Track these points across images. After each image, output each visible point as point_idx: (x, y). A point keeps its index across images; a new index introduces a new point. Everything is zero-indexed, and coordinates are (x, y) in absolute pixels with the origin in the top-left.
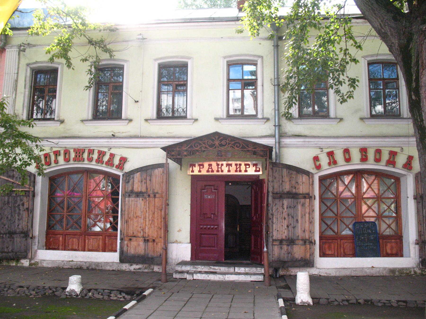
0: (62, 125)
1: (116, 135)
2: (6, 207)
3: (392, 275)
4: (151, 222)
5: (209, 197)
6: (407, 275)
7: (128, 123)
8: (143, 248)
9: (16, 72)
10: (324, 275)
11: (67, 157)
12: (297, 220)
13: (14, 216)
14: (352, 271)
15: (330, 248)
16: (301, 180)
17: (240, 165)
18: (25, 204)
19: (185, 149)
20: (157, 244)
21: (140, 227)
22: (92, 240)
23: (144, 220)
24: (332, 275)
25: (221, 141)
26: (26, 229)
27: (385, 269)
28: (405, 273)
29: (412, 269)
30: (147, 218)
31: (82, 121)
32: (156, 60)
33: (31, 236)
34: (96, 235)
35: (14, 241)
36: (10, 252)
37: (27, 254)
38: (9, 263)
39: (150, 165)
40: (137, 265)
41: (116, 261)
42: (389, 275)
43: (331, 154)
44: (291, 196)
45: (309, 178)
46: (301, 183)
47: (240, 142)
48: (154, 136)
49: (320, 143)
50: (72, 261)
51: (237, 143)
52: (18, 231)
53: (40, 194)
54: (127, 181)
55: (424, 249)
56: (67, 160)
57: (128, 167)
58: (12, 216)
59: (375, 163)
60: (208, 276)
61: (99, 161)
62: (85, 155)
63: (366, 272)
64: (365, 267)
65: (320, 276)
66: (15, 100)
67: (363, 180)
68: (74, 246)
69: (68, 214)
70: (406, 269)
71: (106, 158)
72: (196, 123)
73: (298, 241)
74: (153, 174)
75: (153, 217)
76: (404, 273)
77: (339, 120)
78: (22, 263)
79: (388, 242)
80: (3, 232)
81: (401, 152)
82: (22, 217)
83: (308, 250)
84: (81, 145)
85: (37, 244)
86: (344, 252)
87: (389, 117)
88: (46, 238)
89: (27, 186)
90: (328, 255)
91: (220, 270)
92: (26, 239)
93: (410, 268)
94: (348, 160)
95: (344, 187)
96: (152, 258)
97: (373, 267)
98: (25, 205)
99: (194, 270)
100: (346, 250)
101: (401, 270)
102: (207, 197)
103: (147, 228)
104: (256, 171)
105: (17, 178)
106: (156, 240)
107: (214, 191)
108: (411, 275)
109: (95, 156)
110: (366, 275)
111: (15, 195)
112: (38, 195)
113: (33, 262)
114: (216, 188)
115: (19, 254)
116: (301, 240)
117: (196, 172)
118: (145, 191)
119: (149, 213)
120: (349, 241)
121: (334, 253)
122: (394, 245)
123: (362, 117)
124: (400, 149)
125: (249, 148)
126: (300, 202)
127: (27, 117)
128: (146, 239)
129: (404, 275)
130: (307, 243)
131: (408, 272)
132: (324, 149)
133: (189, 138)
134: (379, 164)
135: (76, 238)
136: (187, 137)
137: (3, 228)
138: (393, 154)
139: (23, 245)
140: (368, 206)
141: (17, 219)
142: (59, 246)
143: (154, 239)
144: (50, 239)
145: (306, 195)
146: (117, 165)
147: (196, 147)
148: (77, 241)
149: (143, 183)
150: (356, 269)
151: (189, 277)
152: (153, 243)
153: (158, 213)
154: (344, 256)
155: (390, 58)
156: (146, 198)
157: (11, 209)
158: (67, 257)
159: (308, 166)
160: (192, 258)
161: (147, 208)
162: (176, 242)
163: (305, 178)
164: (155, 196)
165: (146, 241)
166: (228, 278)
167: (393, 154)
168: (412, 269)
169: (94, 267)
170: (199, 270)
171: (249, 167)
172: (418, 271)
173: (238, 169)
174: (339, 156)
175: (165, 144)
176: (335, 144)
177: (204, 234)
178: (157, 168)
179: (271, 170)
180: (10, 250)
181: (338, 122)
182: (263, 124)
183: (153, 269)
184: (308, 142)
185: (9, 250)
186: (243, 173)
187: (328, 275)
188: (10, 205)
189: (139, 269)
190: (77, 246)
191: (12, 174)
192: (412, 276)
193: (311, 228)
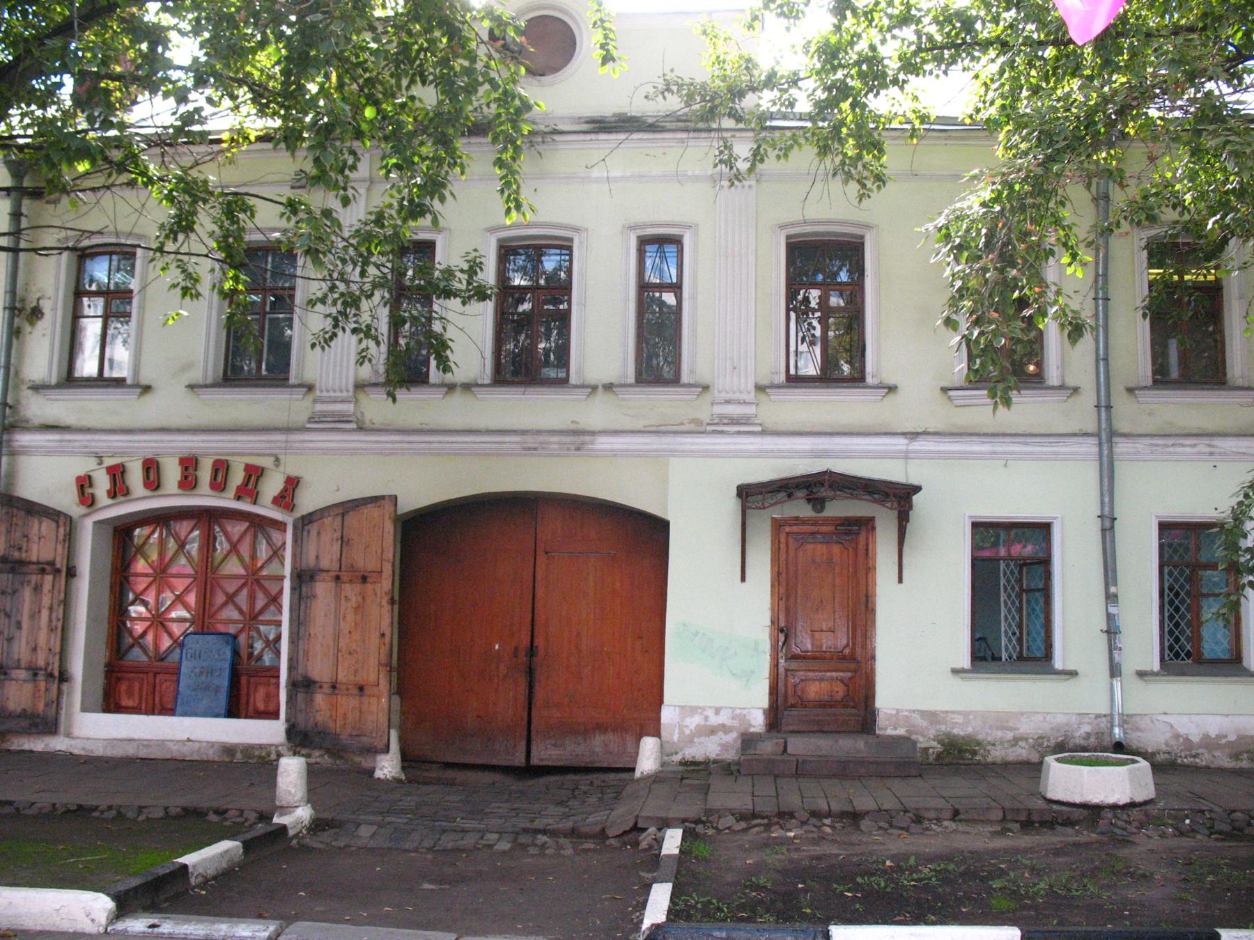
11: (219, 479)
12: (19, 625)
15: (130, 694)
16: (35, 530)
32: (632, 228)
43: (117, 474)
44: (8, 566)
45: (58, 527)
46: (36, 539)
48: (782, 428)
57: (308, 501)
64: (169, 738)
65: (71, 754)
70: (261, 746)
73: (18, 671)
76: (254, 757)
77: (590, 390)
79: (261, 684)
81: (274, 468)
83: (42, 693)
90: (129, 708)
93: (271, 745)
97: (189, 740)
100: (165, 699)
116: (25, 669)
121: (140, 703)
124: (272, 459)
126: (29, 582)
129: (255, 761)
130: (41, 677)
131: (263, 754)
132: (104, 459)
134: (223, 495)
138: (254, 473)
140: (227, 594)
145: (46, 566)
146: (815, 509)
150: (147, 743)
152: (358, 698)
154: (161, 713)
159: (67, 501)
163: (47, 527)
176: (127, 448)
184: (69, 441)
193: (52, 641)
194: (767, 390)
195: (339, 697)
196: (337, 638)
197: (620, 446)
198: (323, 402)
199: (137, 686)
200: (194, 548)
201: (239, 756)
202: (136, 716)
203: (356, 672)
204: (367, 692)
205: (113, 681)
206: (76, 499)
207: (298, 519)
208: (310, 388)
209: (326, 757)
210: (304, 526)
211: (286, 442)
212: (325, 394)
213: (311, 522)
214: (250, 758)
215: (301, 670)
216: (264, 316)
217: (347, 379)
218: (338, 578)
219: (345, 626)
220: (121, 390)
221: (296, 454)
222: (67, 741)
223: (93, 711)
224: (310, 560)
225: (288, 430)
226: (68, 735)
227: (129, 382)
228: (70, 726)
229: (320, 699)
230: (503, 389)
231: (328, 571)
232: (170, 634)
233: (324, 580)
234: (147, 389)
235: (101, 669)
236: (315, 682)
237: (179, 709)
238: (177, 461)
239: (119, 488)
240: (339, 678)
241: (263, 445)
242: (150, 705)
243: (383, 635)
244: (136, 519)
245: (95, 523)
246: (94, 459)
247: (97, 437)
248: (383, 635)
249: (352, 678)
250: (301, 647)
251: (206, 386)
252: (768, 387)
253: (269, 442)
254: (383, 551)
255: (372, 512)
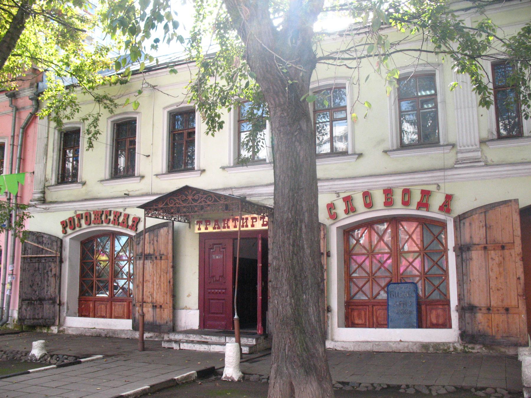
0: (84, 187)
1: (131, 193)
2: (37, 273)
3: (424, 351)
4: (158, 286)
5: (217, 257)
6: (444, 352)
7: (141, 180)
8: (152, 315)
9: (46, 136)
10: (340, 349)
13: (43, 282)
14: (374, 346)
17: (247, 219)
18: (53, 270)
19: (161, 206)
20: (163, 310)
21: (149, 292)
22: (117, 307)
23: (152, 284)
24: (350, 349)
25: (194, 195)
26: (53, 296)
27: (415, 343)
28: (442, 349)
29: (451, 345)
30: (155, 282)
31: (102, 181)
33: (58, 302)
34: (120, 301)
35: (43, 308)
36: (40, 319)
37: (55, 320)
38: (41, 330)
39: (156, 225)
40: (149, 333)
41: (127, 328)
42: (420, 352)
43: (348, 200)
47: (213, 195)
49: (336, 187)
50: (94, 328)
51: (209, 196)
52: (47, 297)
53: (68, 260)
54: (138, 242)
55: (464, 318)
56: (89, 223)
58: (41, 282)
59: (404, 207)
60: (194, 346)
61: (116, 222)
62: (103, 217)
63: (390, 347)
65: (336, 350)
66: (46, 165)
67: (116, 239)
68: (102, 312)
69: (97, 279)
70: (444, 344)
71: (121, 219)
72: (204, 175)
74: (159, 234)
75: (160, 281)
76: (440, 349)
78: (52, 330)
80: (34, 299)
81: (437, 191)
82: (51, 283)
84: (100, 206)
85: (66, 310)
86: (377, 322)
87: (428, 145)
88: (79, 304)
89: (54, 252)
90: (357, 324)
91: (211, 339)
92: (54, 306)
93: (449, 343)
94: (369, 205)
95: (432, 238)
96: (160, 326)
97: (401, 341)
98: (53, 271)
99: (187, 339)
100: (379, 319)
101: (436, 346)
102: (215, 257)
103: (155, 294)
104: (263, 225)
105: (46, 244)
106: (163, 306)
107: (223, 250)
108: (450, 353)
109: (112, 218)
110: (391, 351)
111: (44, 261)
112: (66, 260)
113: (61, 329)
114: (224, 247)
115: (49, 320)
117: (203, 230)
118: (153, 253)
119: (156, 276)
120: (384, 308)
121: (365, 322)
122: (440, 311)
123: (385, 149)
124: (436, 186)
125: (220, 200)
127: (57, 180)
128: (155, 304)
129: (441, 352)
131: (446, 348)
132: (340, 194)
133: (147, 195)
134: (409, 208)
135: (104, 304)
136: (157, 194)
137: (34, 294)
138: (426, 194)
139: (51, 312)
141: (46, 286)
142: (89, 313)
143: (161, 304)
144: (82, 306)
147: (171, 204)
148: (105, 308)
149: (151, 244)
150: (378, 343)
151: (175, 346)
153: (164, 276)
154: (377, 327)
155: (421, 70)
156: (153, 260)
157: (41, 276)
158: (90, 324)
160: (200, 326)
161: (155, 272)
162: (186, 308)
164: (161, 257)
165: (154, 307)
166: (213, 348)
167: (426, 194)
168: (451, 345)
169: (111, 334)
170: (191, 339)
171: (256, 221)
172: (459, 347)
173: (245, 224)
174: (359, 202)
175: (141, 203)
176: (354, 187)
177: (212, 299)
178: (162, 227)
179: (271, 223)
180: (40, 317)
181: (356, 159)
182: (198, 177)
183: (163, 338)
185: (39, 317)
186: (250, 228)
187: (345, 349)
188: (40, 272)
189: (151, 337)
190: (105, 312)
191: (41, 240)
192: (451, 353)
194: (487, 143)
195: (493, 315)
196: (489, 280)
197: (78, 206)
198: (462, 153)
199: (363, 313)
200: (387, 238)
201: (431, 349)
202: (383, 329)
203: (502, 301)
204: (511, 311)
205: (350, 310)
206: (328, 216)
207: (457, 217)
208: (453, 146)
209: (484, 349)
210: (460, 221)
211: (444, 176)
212: (462, 148)
213: (465, 218)
214: (437, 350)
215: (466, 300)
216: (419, 111)
217: (474, 139)
218: (485, 248)
219: (493, 275)
220: (346, 157)
221: (450, 182)
222: (333, 343)
223: (342, 327)
224: (466, 239)
225: (443, 169)
226: (332, 340)
227: (350, 152)
228: (332, 335)
229: (479, 316)
230: (405, 151)
231: (478, 245)
232: (379, 285)
233: (477, 250)
234: (360, 155)
235: (343, 305)
236: (476, 307)
237: (390, 324)
238: (382, 191)
239: (350, 209)
240: (492, 304)
241: (427, 179)
242: (371, 324)
243: (519, 278)
244: (355, 225)
245: (337, 228)
246: (335, 195)
247: (336, 183)
248: (170, 282)
249: (500, 303)
250: (465, 287)
251: (394, 150)
252: (487, 141)
253: (434, 177)
254: (513, 231)
255: (505, 209)
